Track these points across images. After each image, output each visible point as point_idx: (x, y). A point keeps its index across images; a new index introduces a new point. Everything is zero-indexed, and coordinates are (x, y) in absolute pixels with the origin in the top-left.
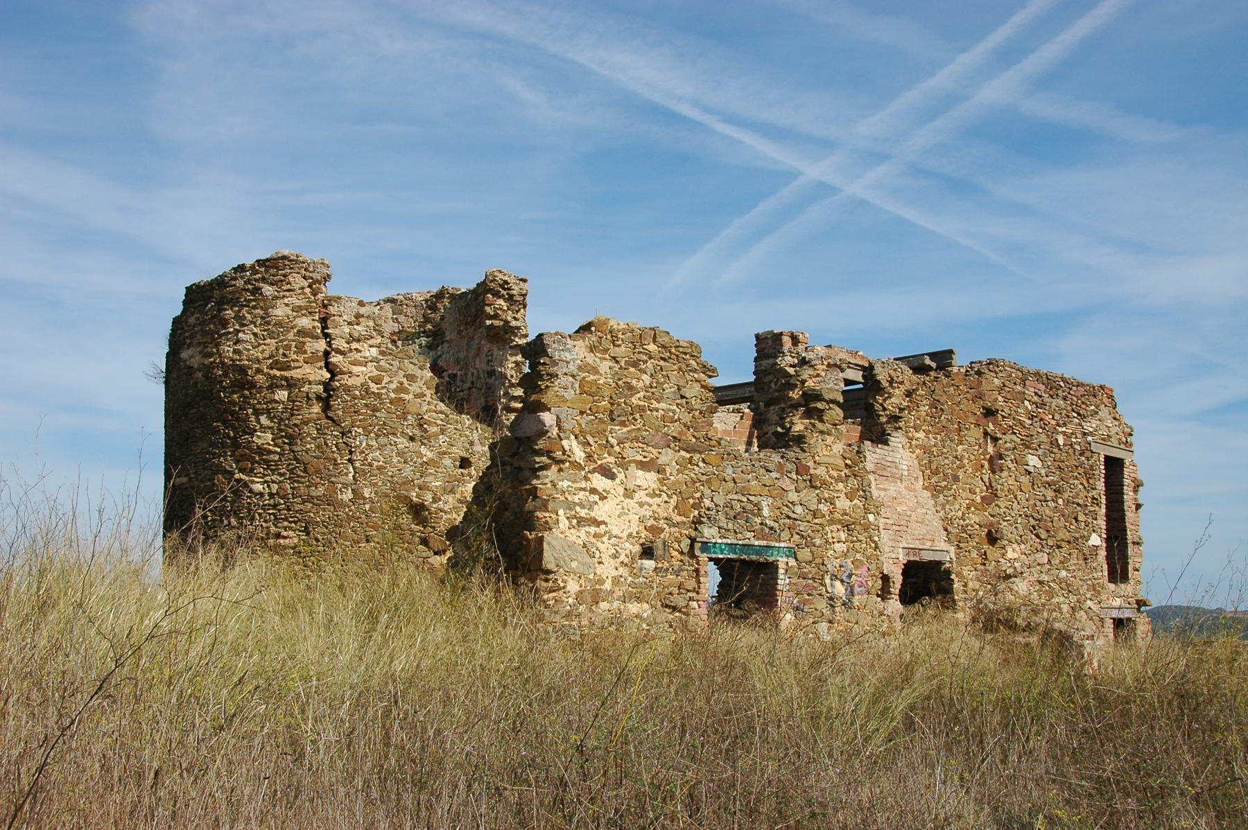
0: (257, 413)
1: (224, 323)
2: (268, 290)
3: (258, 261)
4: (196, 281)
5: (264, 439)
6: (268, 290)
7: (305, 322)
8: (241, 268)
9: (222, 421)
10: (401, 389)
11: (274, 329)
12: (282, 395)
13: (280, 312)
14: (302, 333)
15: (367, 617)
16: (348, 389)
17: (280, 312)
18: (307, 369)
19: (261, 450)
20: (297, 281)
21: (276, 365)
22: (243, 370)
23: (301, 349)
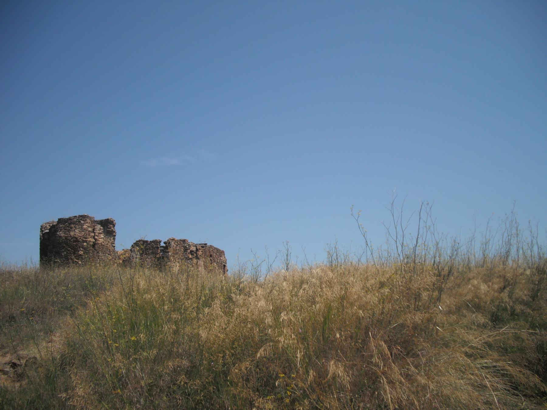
0: (80, 247)
1: (71, 228)
2: (82, 222)
3: (204, 246)
4: (62, 217)
5: (81, 253)
6: (82, 222)
7: (90, 229)
8: (76, 217)
9: (57, 244)
10: (107, 244)
11: (83, 230)
12: (85, 244)
13: (85, 227)
14: (90, 231)
15: (487, 401)
16: (98, 244)
17: (85, 227)
18: (91, 239)
19: (81, 255)
20: (88, 221)
21: (84, 238)
22: (76, 238)
23: (89, 235)
